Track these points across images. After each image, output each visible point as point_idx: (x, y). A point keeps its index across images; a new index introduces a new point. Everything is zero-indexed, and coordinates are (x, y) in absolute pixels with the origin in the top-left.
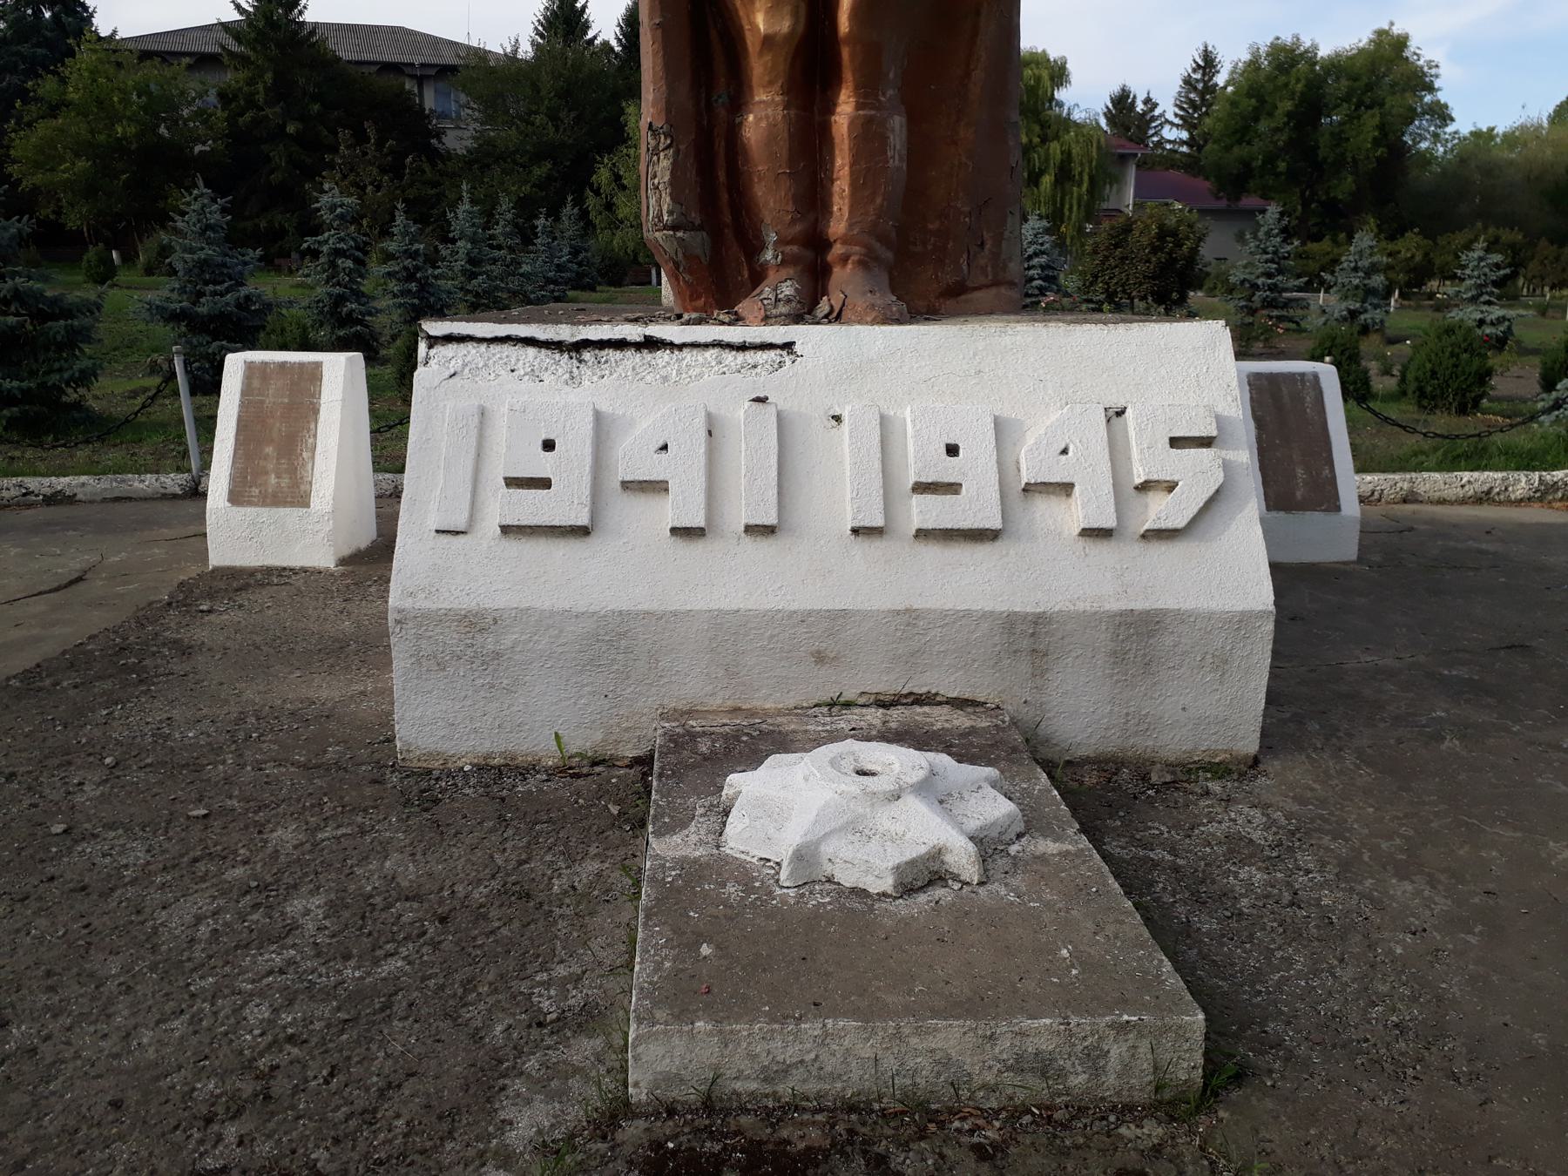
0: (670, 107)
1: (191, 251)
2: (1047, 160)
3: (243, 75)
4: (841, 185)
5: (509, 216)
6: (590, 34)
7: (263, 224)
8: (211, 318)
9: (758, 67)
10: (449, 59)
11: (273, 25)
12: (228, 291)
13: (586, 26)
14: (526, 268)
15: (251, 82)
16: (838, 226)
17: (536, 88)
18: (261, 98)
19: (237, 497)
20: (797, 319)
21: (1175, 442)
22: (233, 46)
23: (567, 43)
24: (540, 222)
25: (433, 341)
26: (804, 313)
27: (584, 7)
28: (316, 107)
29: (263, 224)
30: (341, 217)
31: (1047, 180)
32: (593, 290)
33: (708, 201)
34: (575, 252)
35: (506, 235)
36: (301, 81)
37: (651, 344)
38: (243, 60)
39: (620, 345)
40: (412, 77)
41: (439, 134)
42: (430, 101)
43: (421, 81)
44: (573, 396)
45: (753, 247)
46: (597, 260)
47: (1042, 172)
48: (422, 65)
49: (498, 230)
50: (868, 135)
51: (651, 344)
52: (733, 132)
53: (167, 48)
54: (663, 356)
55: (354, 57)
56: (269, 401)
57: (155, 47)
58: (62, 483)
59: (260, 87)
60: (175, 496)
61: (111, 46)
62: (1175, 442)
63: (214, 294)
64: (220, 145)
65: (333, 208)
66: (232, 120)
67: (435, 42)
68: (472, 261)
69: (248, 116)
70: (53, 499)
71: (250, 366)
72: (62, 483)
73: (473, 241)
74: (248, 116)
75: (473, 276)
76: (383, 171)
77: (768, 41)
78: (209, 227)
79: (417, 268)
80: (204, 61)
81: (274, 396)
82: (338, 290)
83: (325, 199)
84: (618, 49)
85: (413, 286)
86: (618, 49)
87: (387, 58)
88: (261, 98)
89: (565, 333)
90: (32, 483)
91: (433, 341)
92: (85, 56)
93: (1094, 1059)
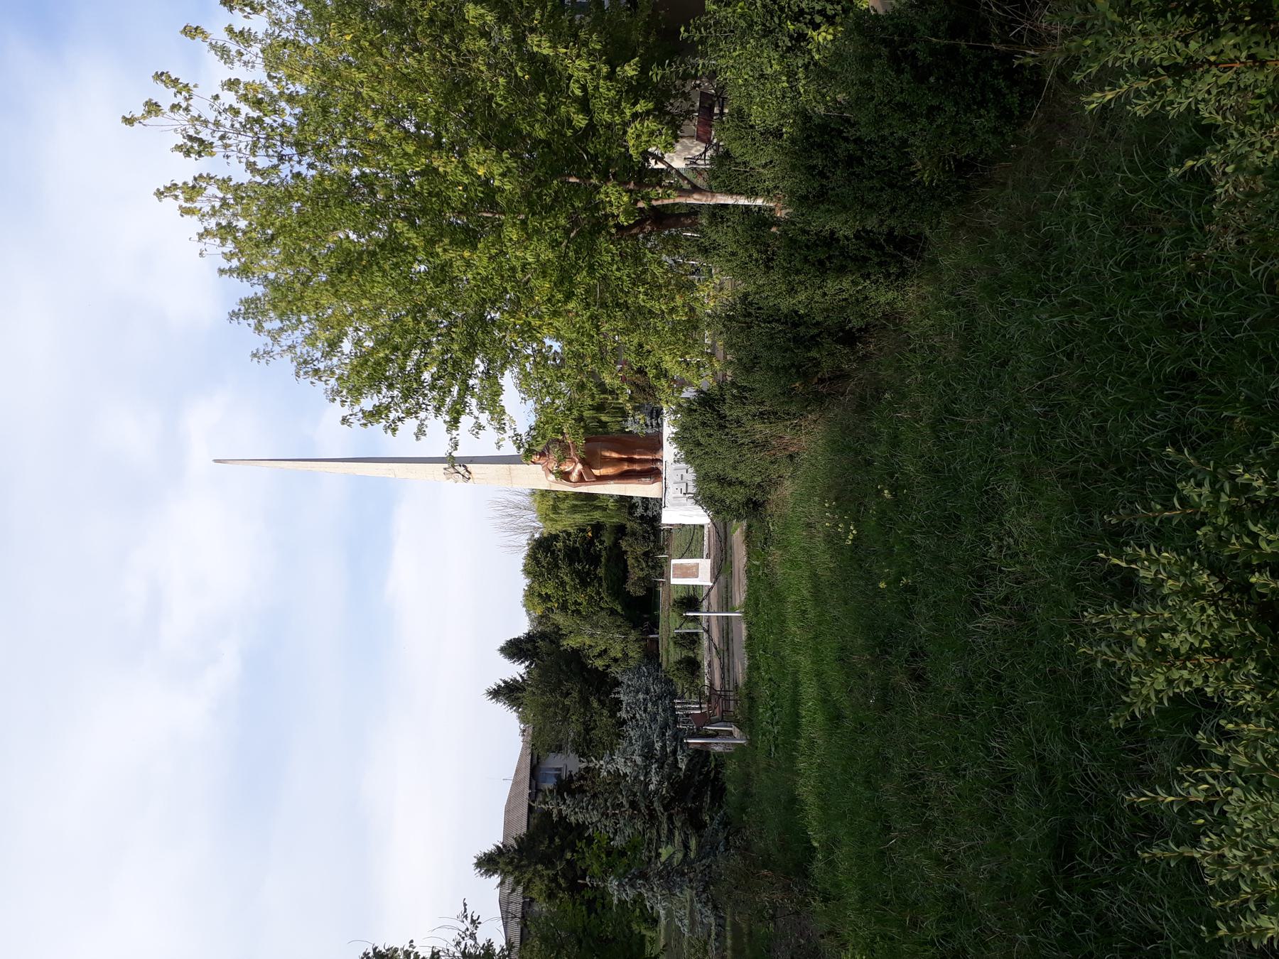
2: (593, 418)
6: (519, 678)
10: (526, 773)
13: (515, 680)
15: (541, 877)
18: (551, 872)
21: (216, 461)
27: (505, 682)
31: (604, 418)
36: (542, 848)
47: (600, 421)
59: (545, 873)
62: (216, 461)
67: (516, 783)
69: (561, 881)
74: (561, 881)
81: (678, 572)
84: (527, 663)
86: (527, 663)
88: (551, 872)
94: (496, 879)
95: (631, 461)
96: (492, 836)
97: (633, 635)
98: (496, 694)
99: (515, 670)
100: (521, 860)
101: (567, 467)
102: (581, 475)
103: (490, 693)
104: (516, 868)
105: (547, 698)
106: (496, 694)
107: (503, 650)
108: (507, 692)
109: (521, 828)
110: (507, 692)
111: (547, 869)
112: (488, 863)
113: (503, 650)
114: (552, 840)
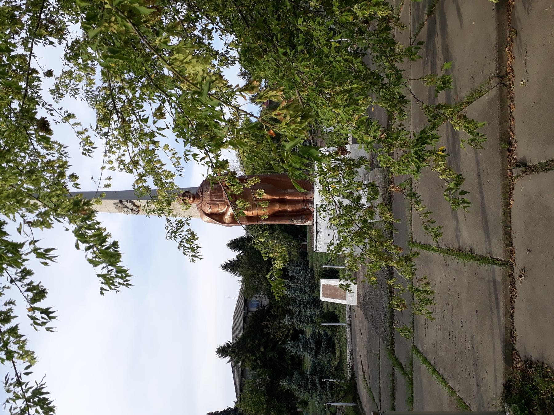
0: (287, 220)
1: (300, 350)
3: (247, 363)
4: (297, 198)
5: (289, 282)
7: (290, 362)
8: (316, 346)
9: (282, 209)
11: (234, 351)
12: (310, 342)
13: (234, 260)
14: (303, 279)
15: (249, 360)
16: (302, 198)
17: (251, 276)
19: (345, 299)
20: (313, 204)
22: (240, 364)
23: (239, 266)
24: (290, 274)
25: (316, 250)
26: (313, 203)
27: (230, 261)
28: (257, 342)
29: (290, 362)
30: (291, 319)
32: (309, 261)
33: (299, 215)
34: (298, 265)
35: (294, 283)
36: (249, 345)
37: (317, 222)
38: (243, 362)
39: (317, 226)
40: (247, 314)
41: (264, 307)
42: (254, 309)
43: (248, 311)
44: (323, 233)
45: (304, 210)
46: (300, 259)
48: (244, 310)
49: (292, 285)
50: (291, 194)
51: (317, 222)
52: (290, 212)
53: (239, 386)
54: (318, 221)
55: (242, 330)
56: (328, 293)
57: (239, 387)
58: (348, 352)
59: (251, 357)
60: (351, 329)
61: (241, 399)
63: (310, 345)
64: (267, 371)
65: (289, 321)
66: (260, 367)
67: (238, 306)
68: (301, 292)
69: (259, 362)
70: (352, 353)
71: (323, 296)
72: (348, 352)
73: (295, 291)
74: (259, 362)
75: (305, 291)
76: (276, 320)
77: (280, 207)
78: (294, 345)
79: (303, 304)
80: (243, 374)
81: (328, 292)
82: (309, 321)
83: (286, 322)
85: (308, 305)
87: (242, 321)
88: (254, 358)
89: (315, 233)
90: (348, 357)
91: (316, 250)
92: (241, 410)
93: (379, 178)
94: (227, 359)
95: (283, 202)
96: (226, 337)
97: (293, 243)
98: (226, 267)
99: (233, 255)
100: (239, 351)
101: (221, 209)
102: (232, 217)
103: (223, 266)
104: (236, 355)
105: (250, 272)
106: (226, 267)
107: (229, 245)
108: (231, 267)
109: (240, 333)
110: (231, 267)
111: (252, 355)
112: (223, 351)
113: (229, 245)
114: (254, 342)
